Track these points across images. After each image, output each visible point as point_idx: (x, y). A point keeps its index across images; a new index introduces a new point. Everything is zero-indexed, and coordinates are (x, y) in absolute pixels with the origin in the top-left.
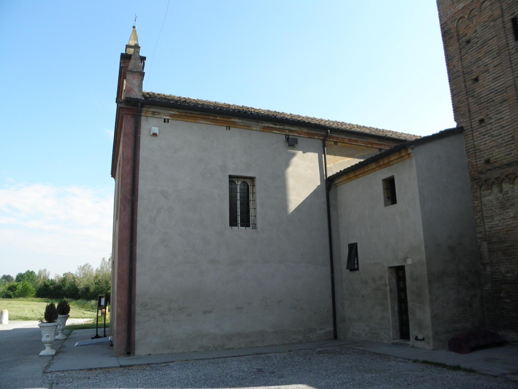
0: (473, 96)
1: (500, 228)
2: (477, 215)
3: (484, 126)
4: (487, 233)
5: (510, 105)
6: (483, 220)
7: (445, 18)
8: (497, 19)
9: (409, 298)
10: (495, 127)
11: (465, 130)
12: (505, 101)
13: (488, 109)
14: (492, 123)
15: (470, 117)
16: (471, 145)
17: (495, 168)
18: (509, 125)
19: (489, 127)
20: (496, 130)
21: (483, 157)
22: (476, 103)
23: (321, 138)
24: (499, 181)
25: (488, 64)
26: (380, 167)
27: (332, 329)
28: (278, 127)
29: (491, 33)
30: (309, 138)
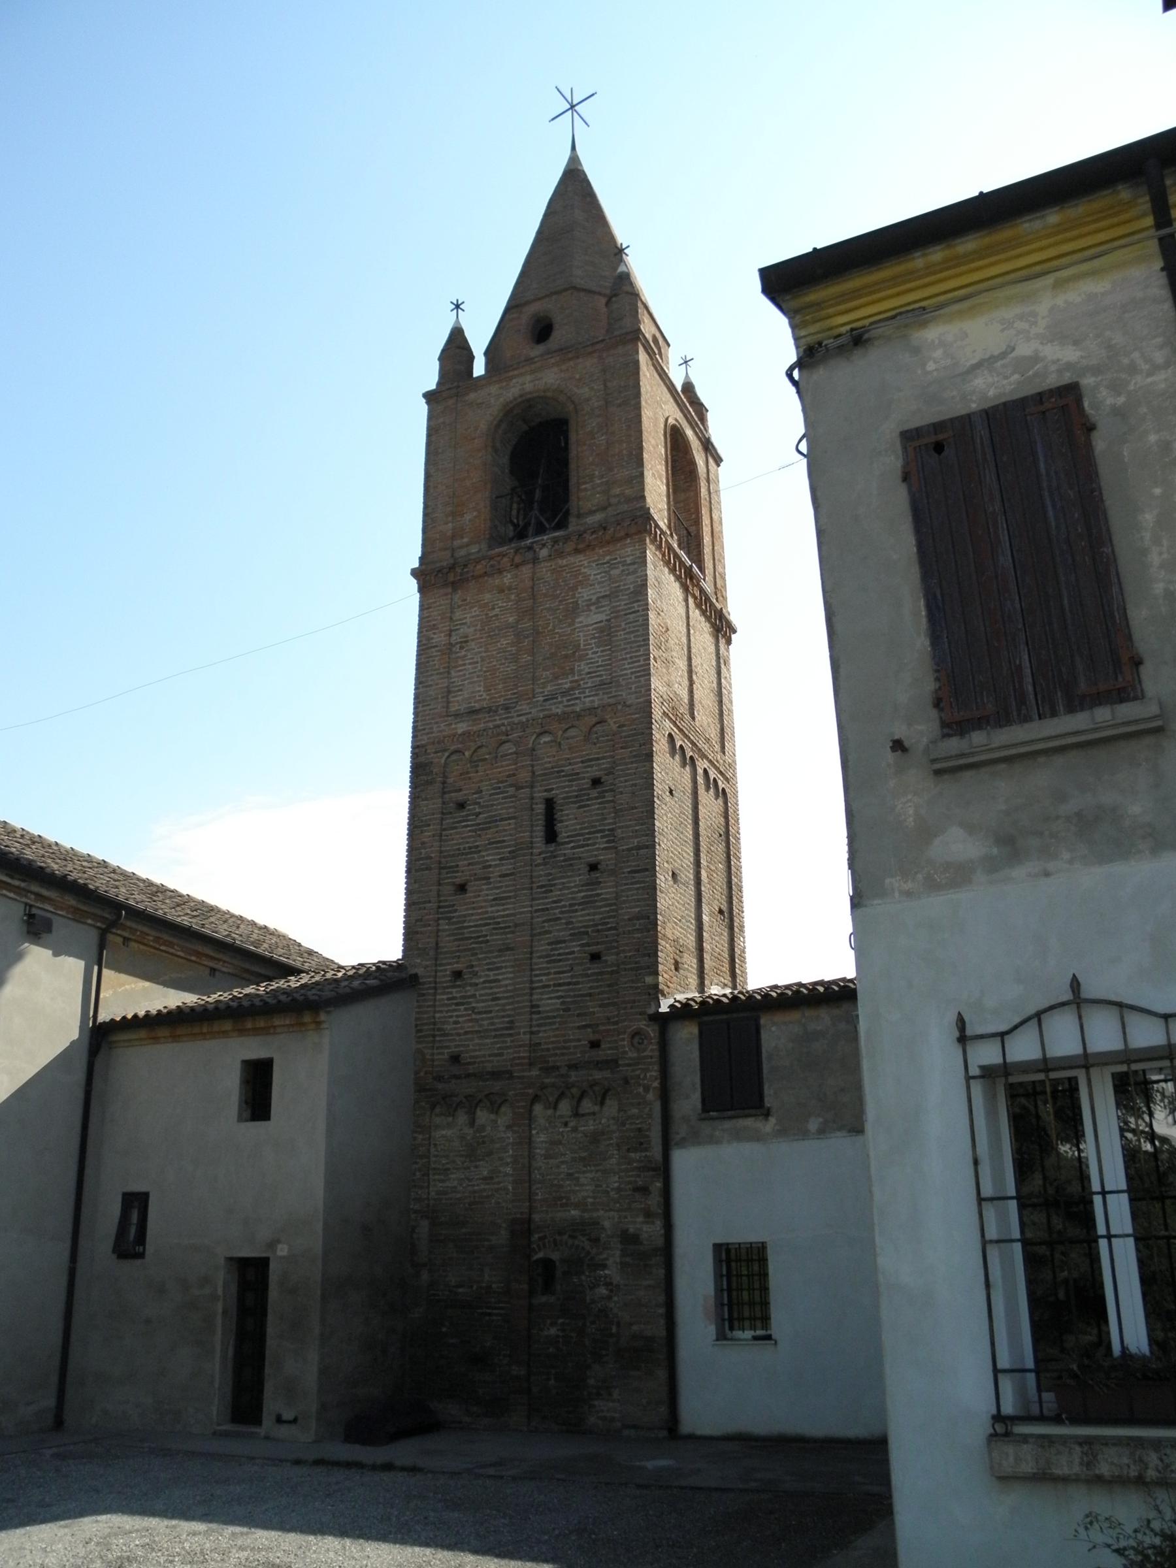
0: (450, 918)
1: (459, 1196)
2: (416, 1163)
3: (459, 986)
4: (432, 1202)
5: (516, 960)
7: (425, 737)
8: (522, 788)
9: (270, 1331)
10: (481, 995)
11: (420, 984)
12: (508, 949)
13: (473, 955)
14: (477, 984)
15: (436, 959)
17: (468, 1076)
18: (507, 998)
19: (470, 991)
20: (483, 1001)
21: (447, 1047)
22: (453, 935)
23: (99, 924)
24: (472, 1104)
25: (490, 866)
26: (242, 1032)
27: (51, 1402)
28: (16, 883)
29: (507, 808)
30: (74, 920)
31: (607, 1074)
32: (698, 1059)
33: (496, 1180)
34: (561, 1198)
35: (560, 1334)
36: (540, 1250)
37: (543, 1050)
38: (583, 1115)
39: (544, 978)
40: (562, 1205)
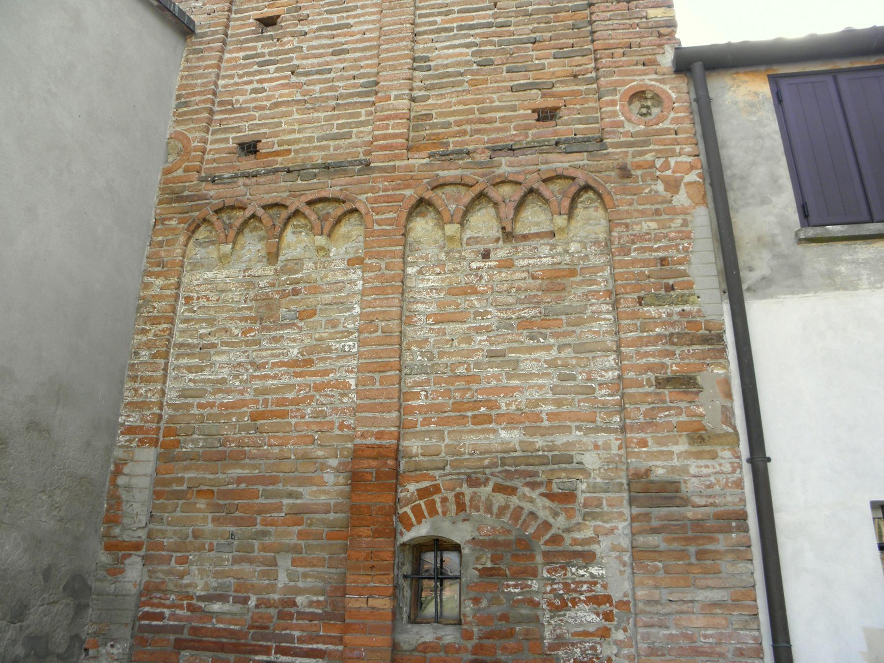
1: (230, 399)
2: (144, 332)
4: (167, 412)
6: (166, 356)
16: (204, 85)
19: (291, 42)
20: (315, 56)
21: (238, 129)
24: (281, 215)
31: (581, 159)
32: (778, 137)
33: (320, 366)
34: (476, 404)
36: (420, 516)
37: (433, 126)
38: (525, 237)
39: (439, 19)
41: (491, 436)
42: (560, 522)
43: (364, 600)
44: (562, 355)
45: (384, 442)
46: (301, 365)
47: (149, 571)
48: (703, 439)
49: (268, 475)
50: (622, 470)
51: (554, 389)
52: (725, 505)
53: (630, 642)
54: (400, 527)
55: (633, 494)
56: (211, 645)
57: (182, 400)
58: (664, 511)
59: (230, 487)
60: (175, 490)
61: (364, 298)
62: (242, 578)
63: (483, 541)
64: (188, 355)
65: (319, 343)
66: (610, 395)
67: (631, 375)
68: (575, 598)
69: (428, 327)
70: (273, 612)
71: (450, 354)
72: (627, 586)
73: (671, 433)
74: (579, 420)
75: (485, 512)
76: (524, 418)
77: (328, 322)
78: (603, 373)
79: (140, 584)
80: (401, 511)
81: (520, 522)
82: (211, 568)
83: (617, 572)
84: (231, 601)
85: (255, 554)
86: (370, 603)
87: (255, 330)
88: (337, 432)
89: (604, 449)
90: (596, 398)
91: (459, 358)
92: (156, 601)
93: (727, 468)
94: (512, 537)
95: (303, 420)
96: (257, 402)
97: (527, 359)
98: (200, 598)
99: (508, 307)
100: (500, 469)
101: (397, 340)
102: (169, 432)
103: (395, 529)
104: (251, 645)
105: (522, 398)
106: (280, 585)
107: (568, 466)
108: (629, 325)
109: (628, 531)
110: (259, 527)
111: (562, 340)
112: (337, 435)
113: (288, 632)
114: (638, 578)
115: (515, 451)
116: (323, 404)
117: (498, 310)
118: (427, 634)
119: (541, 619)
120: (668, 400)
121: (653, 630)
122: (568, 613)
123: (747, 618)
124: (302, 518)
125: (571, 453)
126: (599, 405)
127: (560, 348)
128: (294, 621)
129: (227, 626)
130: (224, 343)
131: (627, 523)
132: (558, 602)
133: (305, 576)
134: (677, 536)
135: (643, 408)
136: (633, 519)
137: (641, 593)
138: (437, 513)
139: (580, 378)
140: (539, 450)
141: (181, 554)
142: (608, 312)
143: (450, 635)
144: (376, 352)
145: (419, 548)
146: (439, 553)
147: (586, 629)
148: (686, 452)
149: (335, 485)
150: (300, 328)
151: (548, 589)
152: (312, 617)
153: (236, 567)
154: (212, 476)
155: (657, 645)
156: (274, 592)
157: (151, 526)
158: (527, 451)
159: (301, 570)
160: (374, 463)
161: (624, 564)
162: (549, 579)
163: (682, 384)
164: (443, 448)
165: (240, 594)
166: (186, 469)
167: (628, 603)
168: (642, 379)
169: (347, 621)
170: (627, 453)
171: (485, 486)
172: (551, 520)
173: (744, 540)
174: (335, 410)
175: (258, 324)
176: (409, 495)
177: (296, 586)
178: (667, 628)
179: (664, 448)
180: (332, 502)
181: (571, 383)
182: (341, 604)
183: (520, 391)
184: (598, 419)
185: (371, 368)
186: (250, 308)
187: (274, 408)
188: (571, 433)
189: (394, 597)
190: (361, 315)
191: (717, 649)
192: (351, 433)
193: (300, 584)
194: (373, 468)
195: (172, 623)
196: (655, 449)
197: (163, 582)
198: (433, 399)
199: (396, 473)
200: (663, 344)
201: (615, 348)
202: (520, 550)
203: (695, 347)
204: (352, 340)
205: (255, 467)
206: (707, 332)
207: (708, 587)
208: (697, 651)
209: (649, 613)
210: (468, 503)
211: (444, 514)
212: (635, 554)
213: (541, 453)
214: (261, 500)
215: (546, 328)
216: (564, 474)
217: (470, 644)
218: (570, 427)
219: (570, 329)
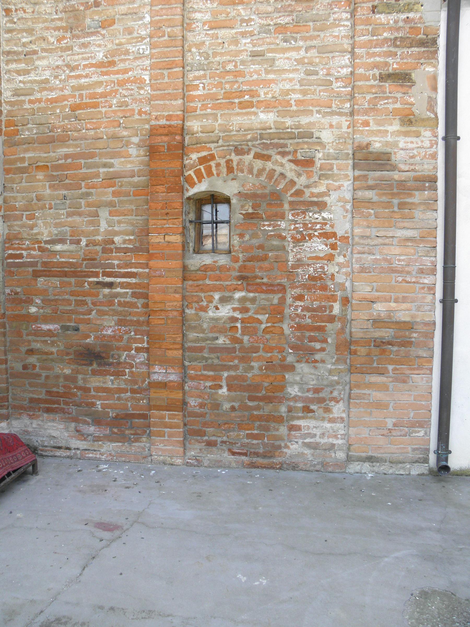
1: (53, 95)
33: (121, 66)
34: (241, 93)
35: (237, 315)
40: (242, 105)
41: (253, 117)
42: (302, 181)
43: (162, 237)
44: (308, 55)
45: (172, 123)
46: (107, 65)
47: (8, 226)
48: (412, 122)
49: (87, 151)
50: (349, 144)
51: (301, 82)
52: (422, 171)
53: (348, 264)
54: (186, 186)
55: (356, 161)
56: (58, 273)
57: (16, 98)
58: (378, 174)
59: (60, 162)
60: (20, 167)
61: (153, 8)
62: (75, 227)
63: (246, 194)
64: (15, 61)
65: (119, 47)
66: (344, 87)
67: (361, 71)
68: (311, 234)
69: (205, 32)
70: (99, 248)
71: (222, 54)
72: (348, 226)
73: (388, 117)
74: (319, 106)
75: (248, 173)
76: (279, 104)
77: (125, 29)
78: (339, 69)
79: (3, 235)
80: (186, 174)
81: (273, 180)
82: (52, 220)
83: (342, 217)
84: (68, 242)
85: (82, 209)
86: (166, 239)
87: (67, 38)
88: (137, 117)
89: (337, 128)
90: (332, 89)
91: (228, 58)
92: (16, 246)
93: (427, 144)
94: (267, 191)
95: (110, 109)
96: (74, 96)
97: (281, 58)
98: (47, 242)
99: (267, 15)
100: (259, 142)
101: (180, 43)
102: (9, 124)
103: (183, 187)
104: (85, 272)
105: (276, 89)
106: (102, 230)
107: (309, 140)
108: (363, 30)
109: (351, 188)
110: (84, 190)
111: (309, 43)
112: (137, 119)
113: (110, 261)
114: (355, 220)
115: (271, 129)
116: (125, 96)
117: (260, 18)
118: (207, 260)
119: (287, 248)
120: (388, 91)
121: (364, 256)
122: (305, 244)
123: (429, 249)
124: (115, 182)
125: (312, 130)
126: (335, 95)
127: (307, 49)
128: (114, 254)
129: (67, 260)
130: (44, 50)
131: (350, 182)
132: (299, 236)
133: (119, 222)
134: (386, 192)
135: (368, 97)
136: (355, 179)
137: (357, 231)
138: (213, 175)
139: (321, 73)
140: (288, 128)
141: (30, 213)
142: (347, 20)
143: (223, 260)
144: (164, 53)
145: (200, 201)
146: (214, 205)
147: (318, 255)
148: (398, 131)
149: (137, 156)
150: (103, 36)
151: (292, 227)
152: (126, 251)
153: (70, 219)
154: (46, 155)
155: (366, 265)
156: (98, 235)
157: (5, 194)
158: (279, 129)
159: (116, 218)
160: (165, 139)
161: (347, 211)
162: (293, 221)
163: (399, 79)
164: (217, 127)
165: (74, 238)
166: (26, 151)
167: (348, 237)
168: (370, 74)
169: (151, 252)
170: (354, 131)
171: (248, 154)
172: (296, 179)
173: (433, 196)
174: (135, 100)
175: (69, 33)
176: (192, 162)
177: (113, 230)
178: (374, 254)
179: (381, 128)
180: (136, 169)
181: (314, 77)
182: (146, 241)
183: (275, 83)
184: (333, 105)
185: (161, 66)
186: (60, 19)
187: (88, 101)
188: (312, 115)
189: (183, 234)
190: (151, 23)
191: (406, 269)
192: (147, 117)
193: (116, 228)
194: (165, 142)
195: (29, 260)
196: (375, 129)
197: (19, 233)
198: (209, 90)
199: (182, 146)
200: (388, 46)
201: (350, 50)
202: (273, 201)
203: (413, 49)
204: (145, 44)
205: (77, 146)
206: (425, 37)
207: (404, 228)
208: (392, 270)
209: (362, 244)
210: (235, 167)
211: (218, 175)
212: (355, 203)
213: (289, 130)
214: (84, 170)
215: (297, 33)
216: (306, 146)
217: (237, 265)
218: (312, 111)
219: (316, 33)
